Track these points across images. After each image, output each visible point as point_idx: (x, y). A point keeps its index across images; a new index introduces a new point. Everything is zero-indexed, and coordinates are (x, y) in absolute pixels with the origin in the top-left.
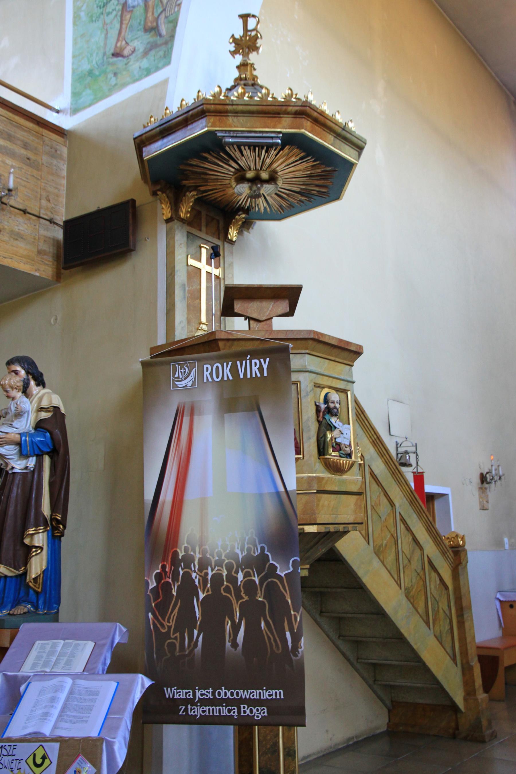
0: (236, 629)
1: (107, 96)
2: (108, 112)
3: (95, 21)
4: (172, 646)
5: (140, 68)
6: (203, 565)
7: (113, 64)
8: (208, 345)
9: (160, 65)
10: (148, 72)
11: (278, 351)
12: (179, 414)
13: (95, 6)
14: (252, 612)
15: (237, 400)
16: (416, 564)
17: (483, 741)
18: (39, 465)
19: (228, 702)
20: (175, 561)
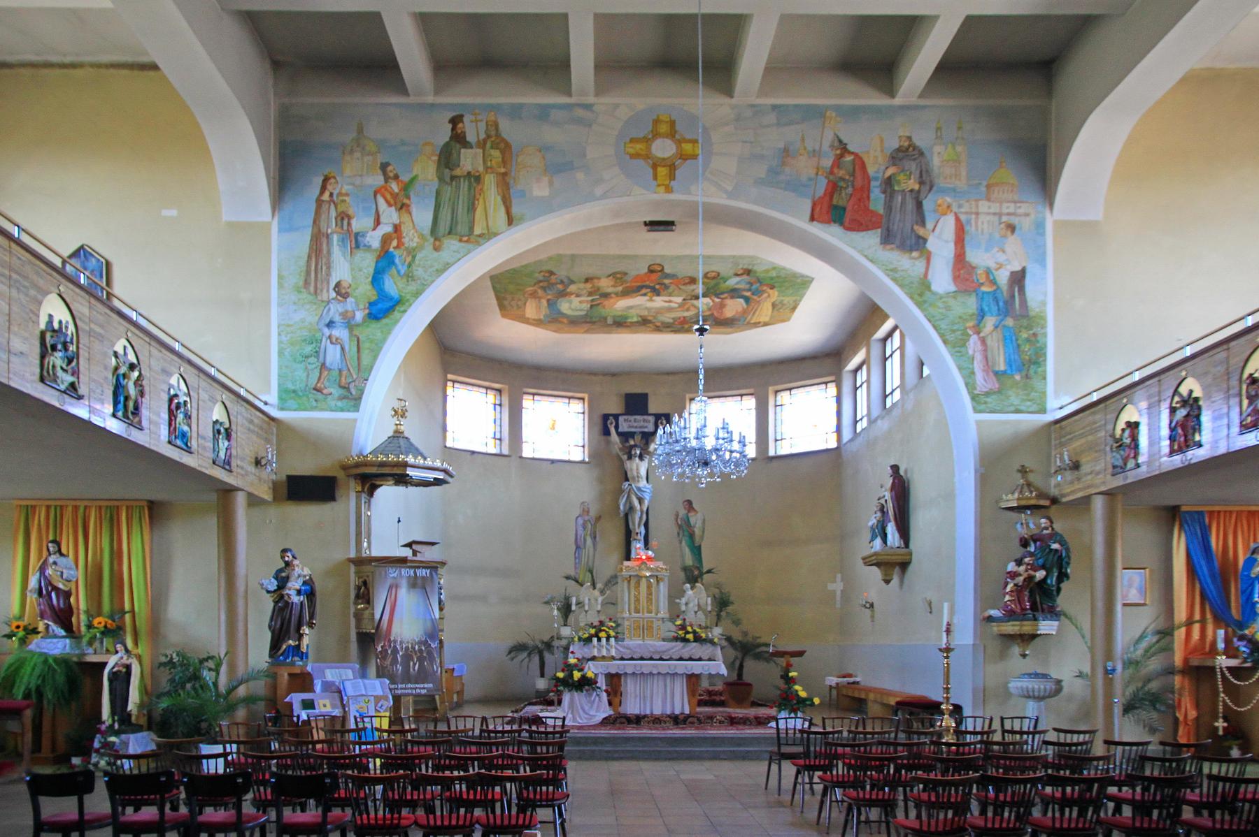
8: (402, 561)
10: (342, 410)
11: (434, 567)
12: (391, 587)
14: (421, 659)
15: (414, 584)
20: (390, 641)
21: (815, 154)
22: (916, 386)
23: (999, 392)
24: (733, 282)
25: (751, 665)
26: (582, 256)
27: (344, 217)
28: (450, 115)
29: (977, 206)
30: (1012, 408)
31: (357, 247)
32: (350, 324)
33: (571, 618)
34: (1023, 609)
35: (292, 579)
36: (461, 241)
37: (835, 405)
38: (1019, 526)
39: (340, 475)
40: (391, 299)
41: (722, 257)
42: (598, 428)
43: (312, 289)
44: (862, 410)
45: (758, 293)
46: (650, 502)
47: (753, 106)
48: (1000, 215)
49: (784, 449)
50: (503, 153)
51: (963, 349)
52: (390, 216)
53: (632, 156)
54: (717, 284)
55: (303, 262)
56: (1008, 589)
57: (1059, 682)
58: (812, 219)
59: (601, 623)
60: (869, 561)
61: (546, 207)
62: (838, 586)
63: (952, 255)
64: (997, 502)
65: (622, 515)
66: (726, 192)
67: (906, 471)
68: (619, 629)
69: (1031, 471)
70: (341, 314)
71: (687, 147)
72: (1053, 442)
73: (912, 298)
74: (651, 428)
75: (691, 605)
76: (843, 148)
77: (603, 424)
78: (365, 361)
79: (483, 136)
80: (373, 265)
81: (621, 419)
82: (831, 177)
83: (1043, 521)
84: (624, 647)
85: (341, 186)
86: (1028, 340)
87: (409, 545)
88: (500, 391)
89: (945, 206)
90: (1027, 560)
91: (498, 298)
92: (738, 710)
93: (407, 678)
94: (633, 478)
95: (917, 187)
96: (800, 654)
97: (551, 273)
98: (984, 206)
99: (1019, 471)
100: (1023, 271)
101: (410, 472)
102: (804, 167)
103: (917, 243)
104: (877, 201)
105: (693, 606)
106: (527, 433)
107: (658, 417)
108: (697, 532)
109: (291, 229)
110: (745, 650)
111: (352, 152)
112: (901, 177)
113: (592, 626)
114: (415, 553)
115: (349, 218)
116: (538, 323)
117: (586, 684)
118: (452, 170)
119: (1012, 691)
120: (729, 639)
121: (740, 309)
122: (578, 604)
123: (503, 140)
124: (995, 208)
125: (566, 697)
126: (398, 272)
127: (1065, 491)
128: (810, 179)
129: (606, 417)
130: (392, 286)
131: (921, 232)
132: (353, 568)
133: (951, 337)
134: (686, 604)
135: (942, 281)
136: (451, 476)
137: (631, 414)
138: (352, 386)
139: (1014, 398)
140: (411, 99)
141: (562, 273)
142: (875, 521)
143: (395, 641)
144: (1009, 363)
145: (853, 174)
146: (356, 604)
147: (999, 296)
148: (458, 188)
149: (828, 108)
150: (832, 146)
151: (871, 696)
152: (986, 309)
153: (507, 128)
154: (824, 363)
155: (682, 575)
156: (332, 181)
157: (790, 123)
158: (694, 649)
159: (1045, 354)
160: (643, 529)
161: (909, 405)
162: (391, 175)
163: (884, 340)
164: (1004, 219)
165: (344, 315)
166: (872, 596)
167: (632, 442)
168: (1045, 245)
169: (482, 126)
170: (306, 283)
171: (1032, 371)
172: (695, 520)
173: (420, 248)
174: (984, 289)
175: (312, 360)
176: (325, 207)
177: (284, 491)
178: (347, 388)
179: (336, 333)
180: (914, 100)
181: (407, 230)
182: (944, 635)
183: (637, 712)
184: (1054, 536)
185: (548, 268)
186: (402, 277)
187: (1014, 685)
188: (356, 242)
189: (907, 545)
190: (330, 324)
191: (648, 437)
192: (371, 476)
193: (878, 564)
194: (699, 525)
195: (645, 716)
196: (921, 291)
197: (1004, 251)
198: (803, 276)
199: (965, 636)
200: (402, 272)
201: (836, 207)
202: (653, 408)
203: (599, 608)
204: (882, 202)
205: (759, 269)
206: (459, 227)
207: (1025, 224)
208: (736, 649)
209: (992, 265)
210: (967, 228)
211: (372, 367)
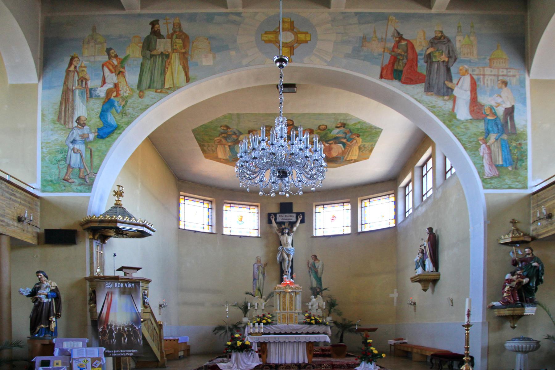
0: (125, 339)
2: (61, 197)
4: (107, 343)
6: (116, 326)
8: (116, 279)
10: (81, 191)
11: (136, 282)
12: (108, 294)
14: (129, 336)
15: (123, 292)
16: (151, 328)
17: (165, 367)
18: (52, 300)
19: (123, 353)
20: (107, 325)
21: (382, 40)
22: (443, 184)
23: (499, 177)
24: (335, 132)
25: (346, 335)
26: (243, 114)
27: (83, 80)
28: (152, 20)
29: (484, 71)
30: (507, 186)
31: (91, 96)
32: (85, 140)
33: (248, 314)
34: (515, 301)
35: (42, 288)
36: (156, 92)
37: (393, 206)
38: (511, 254)
39: (79, 229)
40: (112, 126)
41: (328, 114)
42: (266, 220)
43: (62, 122)
44: (409, 205)
45: (350, 140)
46: (293, 256)
47: (343, 13)
48: (498, 76)
49: (366, 228)
50: (183, 41)
51: (476, 153)
52: (112, 79)
53: (266, 42)
54: (326, 134)
55: (57, 106)
56: (506, 289)
57: (538, 342)
58: (381, 77)
59: (264, 316)
60: (415, 280)
61: (210, 72)
62: (395, 295)
63: (469, 98)
64: (498, 240)
65: (278, 262)
66: (326, 61)
67: (436, 231)
68: (274, 319)
69: (518, 222)
70: (80, 136)
71: (302, 37)
72: (532, 206)
73: (444, 123)
74: (294, 219)
75: (314, 306)
76: (400, 37)
77: (268, 218)
78: (95, 163)
79: (171, 31)
80: (101, 107)
81: (278, 215)
82: (393, 54)
83: (527, 250)
84: (276, 327)
85: (82, 62)
86: (516, 147)
87: (121, 269)
88: (211, 202)
89: (464, 70)
90: (518, 272)
91: (200, 145)
92: (338, 360)
93: (119, 346)
94: (285, 244)
95: (446, 60)
96: (374, 330)
97: (228, 127)
98: (488, 71)
99: (511, 222)
100: (513, 108)
101: (119, 225)
102: (376, 48)
103: (447, 91)
104: (422, 67)
105: (315, 306)
106: (225, 223)
107: (298, 214)
108: (319, 271)
109: (50, 88)
110: (343, 327)
111: (88, 43)
112: (437, 54)
113: (258, 317)
114: (125, 274)
115: (86, 80)
116: (226, 161)
117: (245, 348)
118: (151, 51)
119: (507, 348)
120: (335, 323)
121: (340, 151)
122: (251, 306)
123: (184, 33)
124: (495, 72)
125: (234, 355)
126: (117, 111)
127: (540, 233)
128: (380, 55)
129: (269, 215)
130: (112, 119)
131: (450, 85)
132: (88, 283)
133: (469, 146)
134: (312, 306)
135: (463, 112)
136: (153, 231)
137: (285, 215)
138: (87, 177)
139: (508, 181)
140: (127, 12)
141: (234, 127)
142: (418, 258)
143: (111, 325)
144: (505, 160)
145: (407, 52)
146: (90, 304)
147: (498, 122)
148: (155, 62)
149: (390, 14)
150: (393, 36)
151: (415, 350)
152: (491, 129)
153: (186, 27)
154: (388, 184)
155: (310, 291)
156: (76, 59)
157: (367, 23)
158: (315, 328)
159: (526, 155)
160: (290, 270)
161: (439, 195)
162: (113, 55)
163: (422, 167)
164: (500, 78)
165: (82, 136)
166: (415, 299)
167: (283, 227)
168: (525, 93)
169: (171, 27)
170: (59, 118)
171: (518, 165)
172: (318, 265)
173: (131, 96)
174: (489, 118)
175: (62, 162)
176: (71, 74)
177: (43, 239)
178: (84, 179)
179: (77, 146)
180: (444, 11)
181: (123, 87)
182: (466, 317)
183: (277, 362)
184: (533, 259)
185: (225, 123)
186: (119, 114)
187: (509, 345)
188: (90, 94)
189: (437, 270)
190: (74, 142)
191: (292, 224)
192: (101, 230)
193: (420, 281)
194: (320, 267)
195: (281, 365)
196: (450, 119)
197: (501, 97)
198: (376, 128)
199: (478, 318)
200: (119, 111)
201: (396, 71)
202: (295, 209)
203: (263, 308)
204: (425, 68)
205: (351, 123)
206: (155, 85)
207: (513, 81)
208: (339, 328)
209: (493, 103)
210: (478, 83)
211: (100, 166)
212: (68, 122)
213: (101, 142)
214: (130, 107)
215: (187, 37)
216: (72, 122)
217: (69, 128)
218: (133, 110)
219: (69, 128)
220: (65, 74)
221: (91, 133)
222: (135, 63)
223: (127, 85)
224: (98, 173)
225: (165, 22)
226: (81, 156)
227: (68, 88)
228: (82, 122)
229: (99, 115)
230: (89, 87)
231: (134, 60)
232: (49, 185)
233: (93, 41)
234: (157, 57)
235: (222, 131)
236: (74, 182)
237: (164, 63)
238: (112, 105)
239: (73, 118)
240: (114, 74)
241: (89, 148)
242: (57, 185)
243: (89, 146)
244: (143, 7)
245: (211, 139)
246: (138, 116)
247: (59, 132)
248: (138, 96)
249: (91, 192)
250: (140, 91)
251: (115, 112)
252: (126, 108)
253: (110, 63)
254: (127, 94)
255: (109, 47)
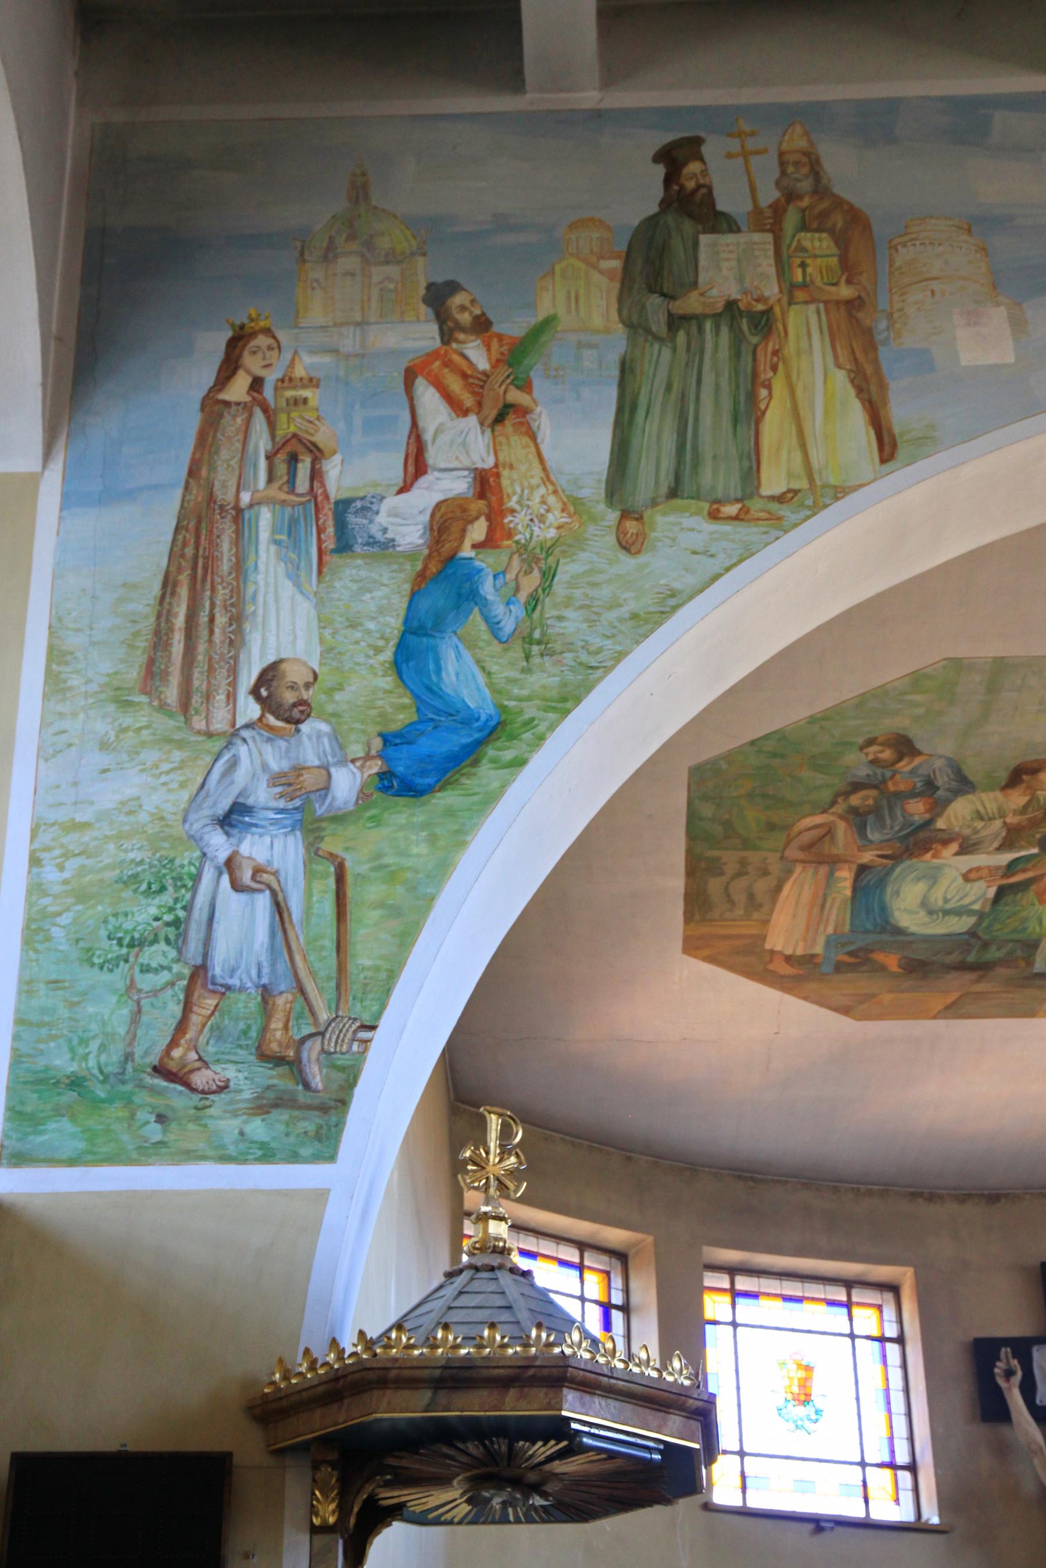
1: (130, 1162)
3: (101, 968)
5: (242, 1133)
7: (153, 1090)
9: (305, 1152)
10: (267, 1155)
13: (103, 933)
27: (297, 453)
31: (344, 546)
36: (714, 516)
39: (247, 1446)
40: (468, 719)
42: (961, 1394)
43: (172, 694)
50: (842, 241)
52: (460, 445)
70: (277, 779)
78: (365, 956)
79: (769, 195)
88: (621, 1256)
97: (904, 746)
111: (329, 254)
115: (317, 453)
123: (839, 203)
126: (494, 627)
129: (984, 1352)
130: (466, 673)
138: (312, 1051)
153: (845, 169)
156: (262, 341)
162: (465, 318)
165: (288, 782)
170: (152, 674)
173: (568, 542)
175: (158, 954)
176: (232, 423)
178: (294, 1066)
179: (254, 848)
188: (339, 532)
190: (234, 818)
200: (508, 626)
206: (707, 477)
211: (393, 976)
212: (208, 697)
213: (403, 815)
214: (568, 602)
215: (856, 218)
216: (231, 697)
217: (209, 735)
218: (592, 623)
219: (209, 735)
220: (193, 420)
221: (342, 762)
222: (589, 357)
223: (547, 478)
224: (384, 1024)
225: (734, 145)
226: (279, 908)
227: (211, 498)
228: (289, 697)
229: (388, 655)
230: (334, 494)
231: (580, 345)
232: (58, 1112)
233: (355, 246)
234: (708, 325)
235: (863, 772)
236: (224, 1088)
237: (747, 359)
238: (467, 595)
239: (234, 672)
240: (472, 420)
241: (332, 857)
242: (116, 1111)
243: (328, 845)
244: (610, 78)
245: (771, 827)
246: (619, 657)
247: (151, 756)
248: (611, 539)
249: (332, 1158)
250: (625, 515)
251: (486, 636)
252: (549, 610)
253: (448, 364)
254: (552, 533)
255: (440, 279)
